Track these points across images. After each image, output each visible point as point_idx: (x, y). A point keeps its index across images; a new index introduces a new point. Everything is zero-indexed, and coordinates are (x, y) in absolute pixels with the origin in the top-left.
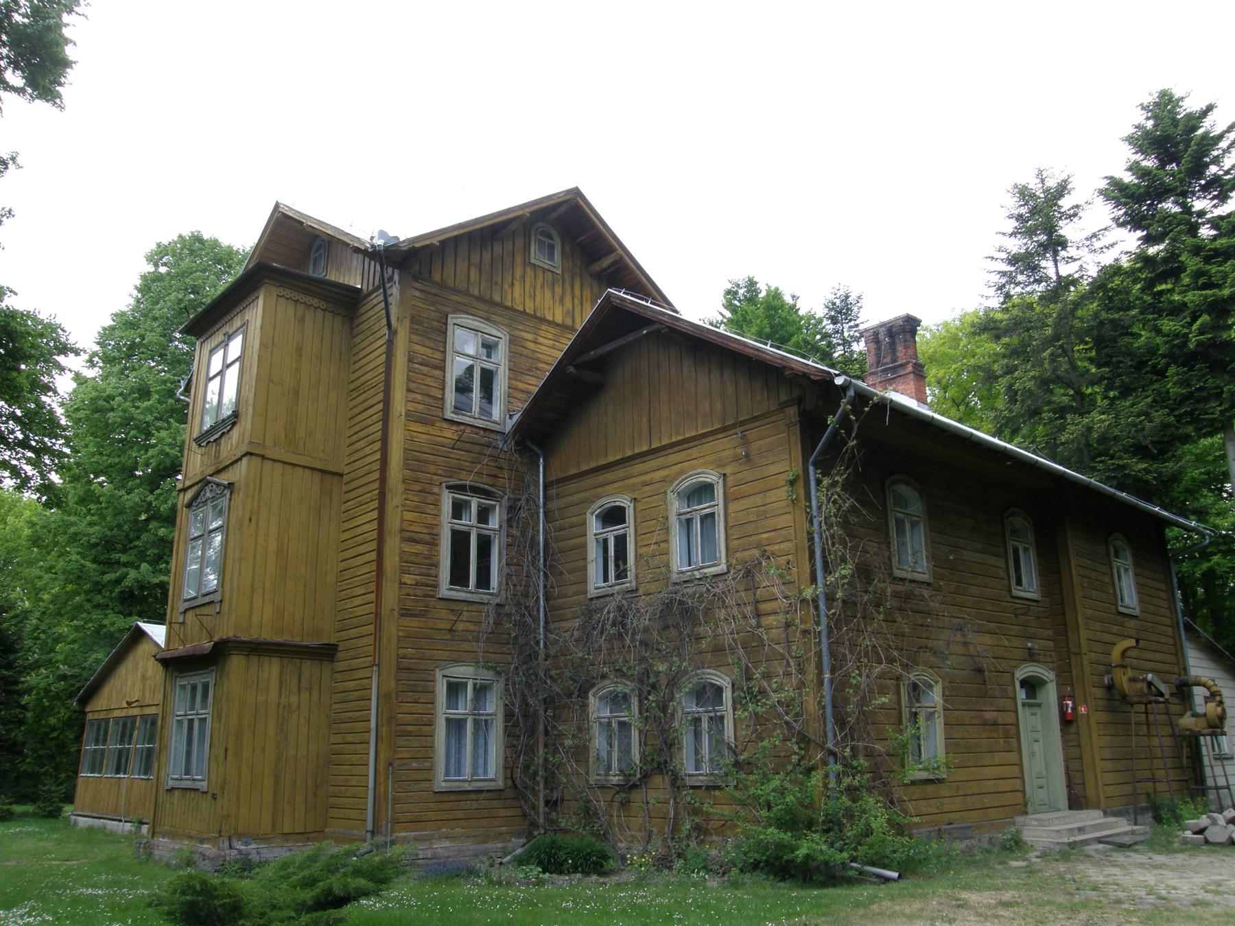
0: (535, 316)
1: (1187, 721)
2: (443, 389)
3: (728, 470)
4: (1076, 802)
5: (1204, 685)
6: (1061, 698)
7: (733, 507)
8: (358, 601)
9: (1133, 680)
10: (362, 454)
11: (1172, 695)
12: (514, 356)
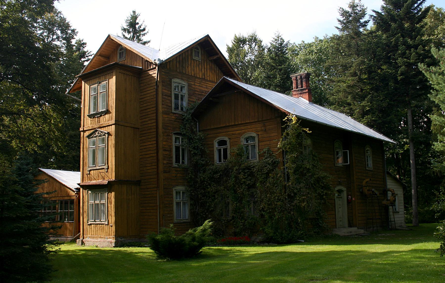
0: (195, 77)
1: (385, 202)
2: (171, 103)
3: (259, 133)
4: (350, 225)
5: (391, 191)
6: (348, 196)
7: (260, 144)
8: (148, 168)
9: (368, 190)
10: (146, 123)
11: (380, 194)
12: (189, 90)
